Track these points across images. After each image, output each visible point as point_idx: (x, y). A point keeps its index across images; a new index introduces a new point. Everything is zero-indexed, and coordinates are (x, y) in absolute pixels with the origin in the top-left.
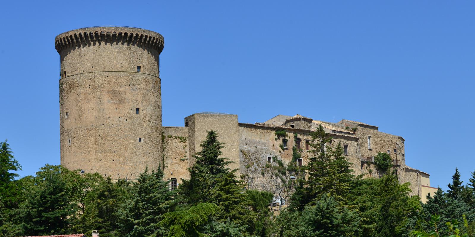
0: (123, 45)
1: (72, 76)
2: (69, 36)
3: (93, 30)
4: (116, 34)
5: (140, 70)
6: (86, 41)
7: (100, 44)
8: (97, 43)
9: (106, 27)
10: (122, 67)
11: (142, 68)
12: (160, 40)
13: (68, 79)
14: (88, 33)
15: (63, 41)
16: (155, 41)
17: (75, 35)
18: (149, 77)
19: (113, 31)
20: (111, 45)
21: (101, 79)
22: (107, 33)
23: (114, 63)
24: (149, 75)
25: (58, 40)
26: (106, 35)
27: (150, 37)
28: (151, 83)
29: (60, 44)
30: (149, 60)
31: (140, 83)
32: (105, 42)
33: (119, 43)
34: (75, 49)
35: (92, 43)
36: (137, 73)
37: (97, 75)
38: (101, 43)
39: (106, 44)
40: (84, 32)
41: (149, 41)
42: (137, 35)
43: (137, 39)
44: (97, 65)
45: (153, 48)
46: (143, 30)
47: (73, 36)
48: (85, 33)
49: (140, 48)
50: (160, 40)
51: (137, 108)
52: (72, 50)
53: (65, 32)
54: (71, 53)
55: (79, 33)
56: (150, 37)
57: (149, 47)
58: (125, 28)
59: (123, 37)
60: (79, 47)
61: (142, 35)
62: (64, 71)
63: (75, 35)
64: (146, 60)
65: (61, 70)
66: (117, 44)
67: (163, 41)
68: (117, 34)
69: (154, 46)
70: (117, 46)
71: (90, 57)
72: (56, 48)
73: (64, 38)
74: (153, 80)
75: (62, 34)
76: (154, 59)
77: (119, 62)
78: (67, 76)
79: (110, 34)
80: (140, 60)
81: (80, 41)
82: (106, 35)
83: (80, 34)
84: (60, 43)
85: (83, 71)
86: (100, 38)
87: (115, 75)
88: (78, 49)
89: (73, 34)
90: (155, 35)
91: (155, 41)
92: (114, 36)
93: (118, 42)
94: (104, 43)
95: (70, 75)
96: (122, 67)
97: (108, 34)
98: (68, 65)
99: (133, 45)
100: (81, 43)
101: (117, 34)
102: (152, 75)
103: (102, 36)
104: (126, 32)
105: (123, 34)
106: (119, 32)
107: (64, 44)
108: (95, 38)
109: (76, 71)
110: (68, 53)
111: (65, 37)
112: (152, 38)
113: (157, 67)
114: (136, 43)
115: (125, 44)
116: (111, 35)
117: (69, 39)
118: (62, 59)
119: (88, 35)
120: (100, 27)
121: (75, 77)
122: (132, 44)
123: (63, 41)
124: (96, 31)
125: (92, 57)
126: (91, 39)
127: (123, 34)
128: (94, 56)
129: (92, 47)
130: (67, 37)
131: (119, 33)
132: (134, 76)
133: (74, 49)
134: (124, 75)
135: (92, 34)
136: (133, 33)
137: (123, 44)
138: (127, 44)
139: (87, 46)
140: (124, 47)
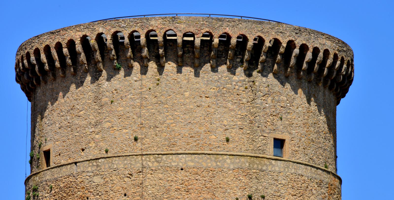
0: (234, 74)
1: (69, 166)
2: (66, 41)
3: (142, 27)
4: (211, 41)
5: (282, 153)
6: (117, 59)
7: (161, 68)
8: (152, 66)
9: (183, 18)
10: (228, 140)
11: (287, 146)
12: (342, 58)
13: (57, 173)
14: (126, 34)
15: (43, 57)
16: (329, 62)
17: (84, 40)
18: (308, 172)
19: (203, 31)
20: (197, 75)
21: (161, 176)
22: (185, 35)
23: (203, 129)
24: (309, 168)
25: (28, 54)
26: (180, 40)
27: (316, 51)
28: (314, 192)
29: (34, 65)
30: (310, 121)
31: (282, 191)
32: (177, 62)
33: (220, 69)
34: (82, 82)
35: (136, 66)
36: (273, 162)
37: (151, 163)
38: (147, 67)
39: (179, 71)
40: (113, 30)
41: (311, 63)
42: (277, 43)
43: (277, 57)
44: (151, 132)
45: (320, 85)
46: (295, 29)
47: (78, 42)
48: (115, 36)
49: (283, 84)
50: (342, 58)
51: (276, 140)
52: (73, 87)
53: (53, 30)
54: (68, 95)
55: (96, 33)
56: (316, 51)
57: (309, 82)
58: (239, 20)
59: (233, 49)
60: (96, 78)
61: (291, 45)
62: (46, 148)
63: (84, 40)
64: (299, 121)
65: (33, 148)
66: (214, 69)
67: (350, 64)
68: (216, 41)
69: (326, 78)
70: (215, 76)
71: (128, 109)
72: (19, 79)
73: (47, 49)
74: (320, 184)
75: (41, 35)
76: (325, 119)
77: (218, 124)
78: (52, 165)
79: (192, 39)
80: (281, 119)
81: (100, 59)
82: (180, 40)
83: (100, 38)
84: (35, 62)
85: (107, 152)
86: (161, 51)
87: (204, 165)
88: (92, 82)
89: (77, 36)
90: (323, 40)
91: (329, 62)
92: (207, 44)
93: (218, 65)
94: (175, 66)
95: (63, 162)
96: (228, 140)
97: (186, 39)
98: (58, 131)
99: (264, 73)
100: (101, 65)
101: (216, 41)
102: (318, 168)
103: (169, 44)
104: (243, 32)
105: (234, 41)
106: (221, 33)
107: (47, 67)
108: (145, 52)
109: (83, 150)
110: (61, 94)
111: (53, 46)
112: (321, 54)
113: (332, 142)
114: (273, 66)
115: (240, 70)
116: (198, 42)
117: (65, 51)
118: (37, 112)
119: (127, 40)
120: (163, 17)
121: (81, 167)
122: (259, 72)
123: (43, 57)
124: (151, 28)
125: (134, 107)
126: (133, 52)
127: (234, 41)
128: (141, 105)
129: (135, 78)
130: (59, 46)
131: (221, 36)
132: (264, 168)
133: (80, 84)
134: (232, 167)
135: (139, 37)
136: (262, 35)
137: (232, 70)
138: (245, 71)
139: (122, 73)
140: (235, 78)
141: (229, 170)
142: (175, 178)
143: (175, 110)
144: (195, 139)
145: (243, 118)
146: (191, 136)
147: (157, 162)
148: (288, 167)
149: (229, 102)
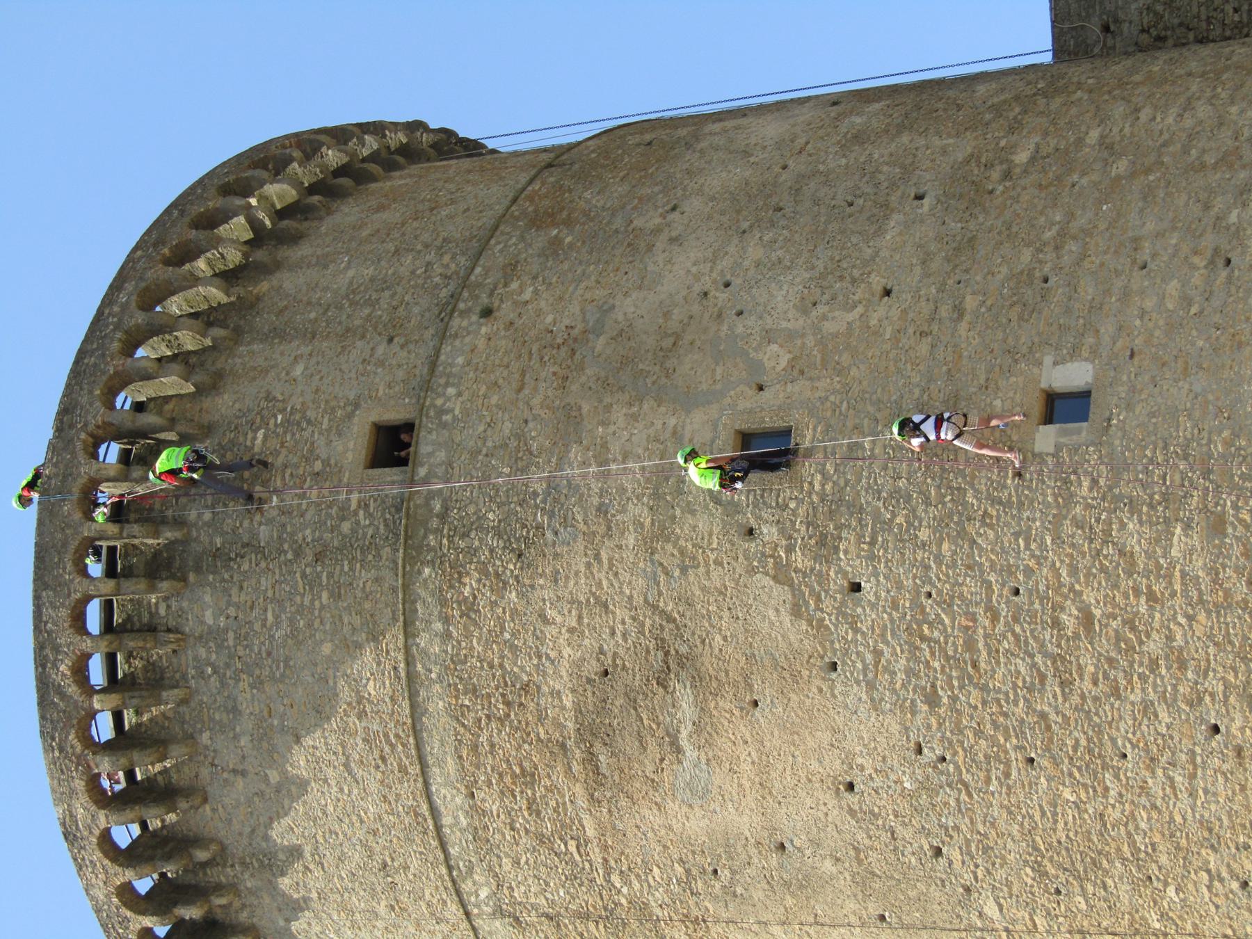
134: (438, 626)
141: (448, 635)
142: (502, 816)
143: (324, 813)
144: (387, 749)
145: (312, 583)
146: (380, 762)
147: (471, 870)
148: (442, 411)
149: (273, 636)
